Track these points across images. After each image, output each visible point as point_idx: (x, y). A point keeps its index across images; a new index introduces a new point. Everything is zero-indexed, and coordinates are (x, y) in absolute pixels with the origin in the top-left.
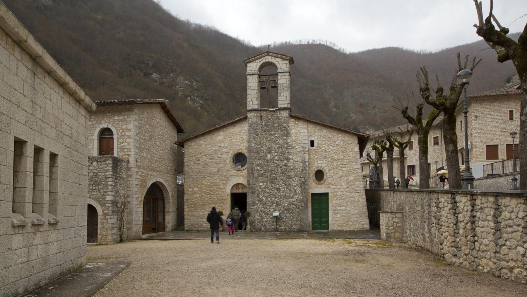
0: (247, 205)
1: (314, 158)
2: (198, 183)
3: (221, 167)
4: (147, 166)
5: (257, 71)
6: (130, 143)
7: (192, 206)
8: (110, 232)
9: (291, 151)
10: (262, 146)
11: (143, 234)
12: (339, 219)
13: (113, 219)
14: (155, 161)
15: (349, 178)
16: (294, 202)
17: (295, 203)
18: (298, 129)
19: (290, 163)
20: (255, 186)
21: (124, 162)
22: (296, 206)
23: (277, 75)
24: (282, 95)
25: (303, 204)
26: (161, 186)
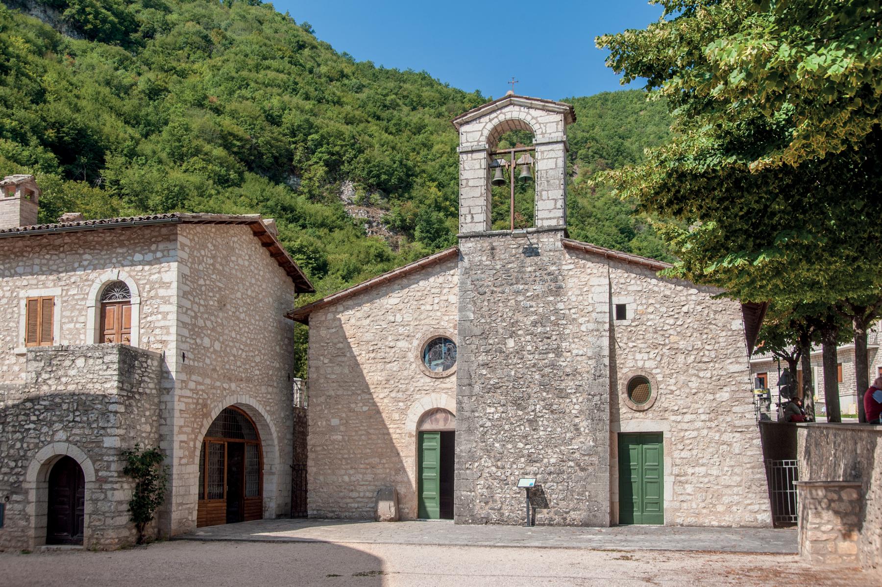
0: (456, 460)
3: (394, 369)
4: (211, 367)
5: (484, 144)
6: (167, 313)
8: (111, 521)
9: (567, 331)
10: (493, 318)
11: (199, 525)
12: (689, 498)
13: (121, 492)
14: (234, 356)
15: (718, 396)
18: (584, 278)
19: (562, 359)
20: (476, 414)
21: (152, 360)
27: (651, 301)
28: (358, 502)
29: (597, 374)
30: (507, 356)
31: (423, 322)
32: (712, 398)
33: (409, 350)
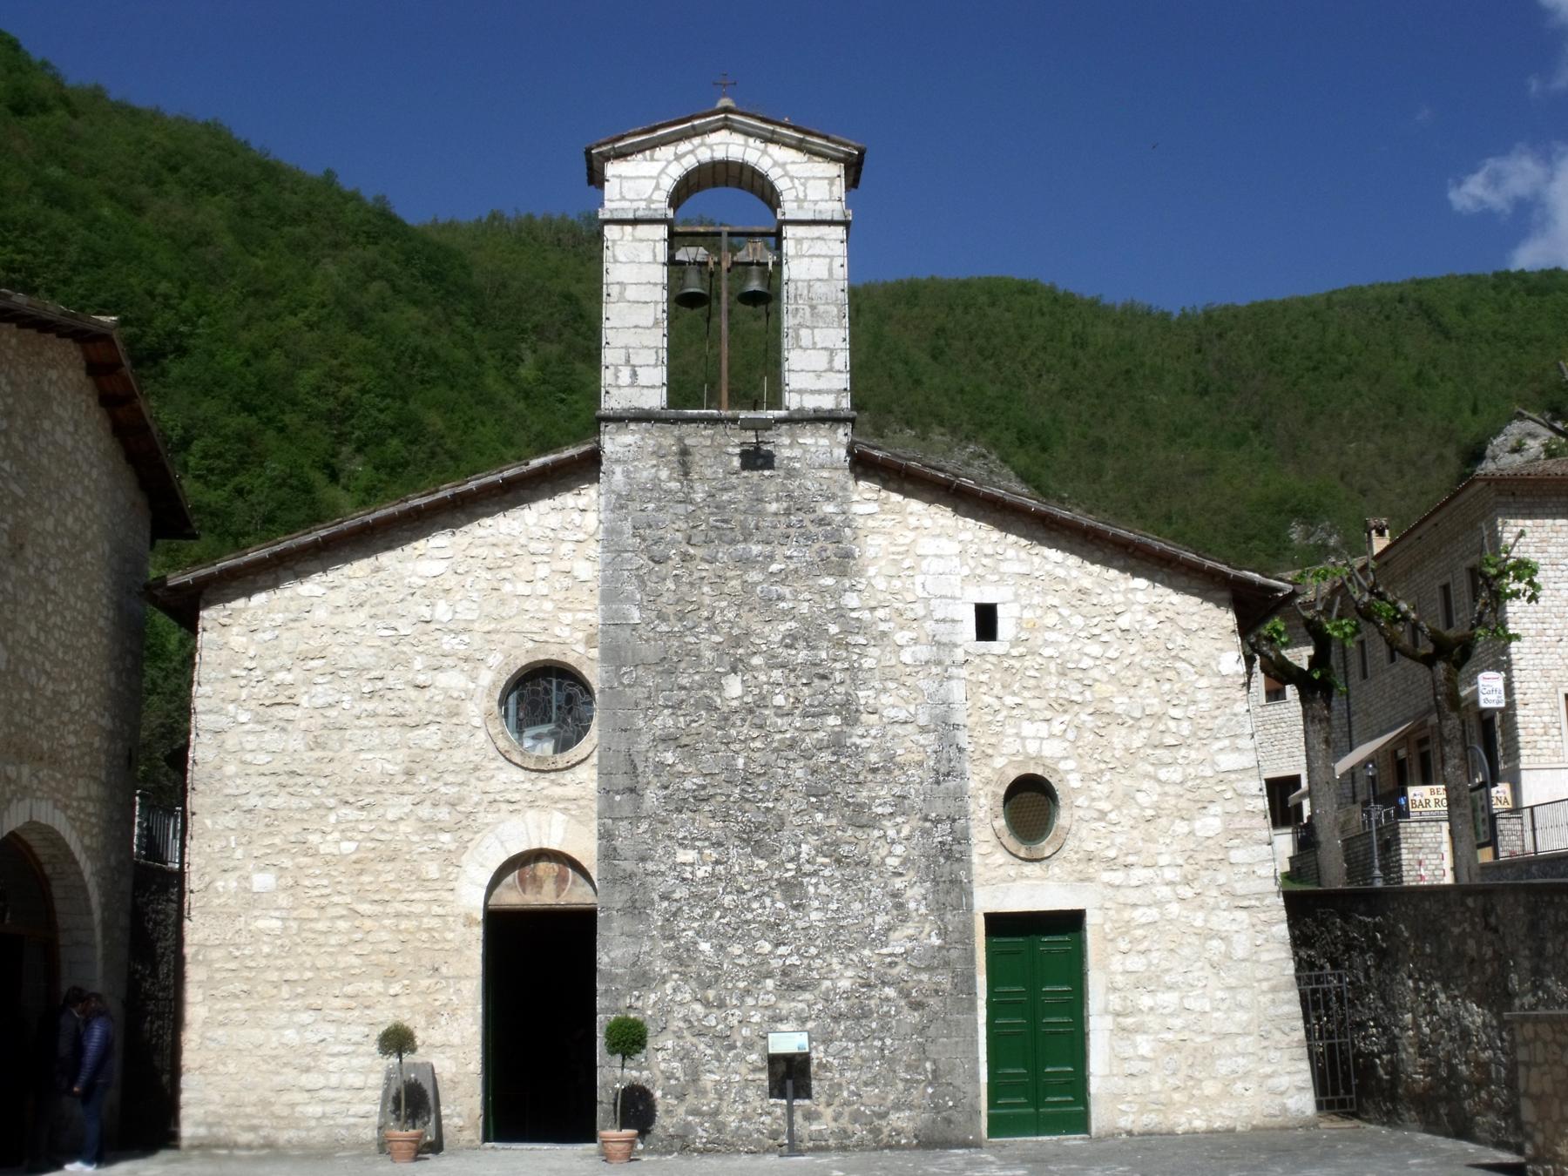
0: (600, 987)
1: (996, 704)
2: (277, 840)
3: (428, 744)
5: (661, 206)
7: (237, 987)
9: (868, 663)
12: (1146, 1066)
15: (1197, 824)
16: (892, 965)
17: (895, 971)
19: (861, 731)
20: (650, 866)
22: (906, 994)
23: (778, 236)
24: (803, 343)
25: (944, 980)
26: (43, 859)
28: (325, 1101)
29: (943, 770)
30: (726, 719)
31: (505, 625)
32: (1186, 830)
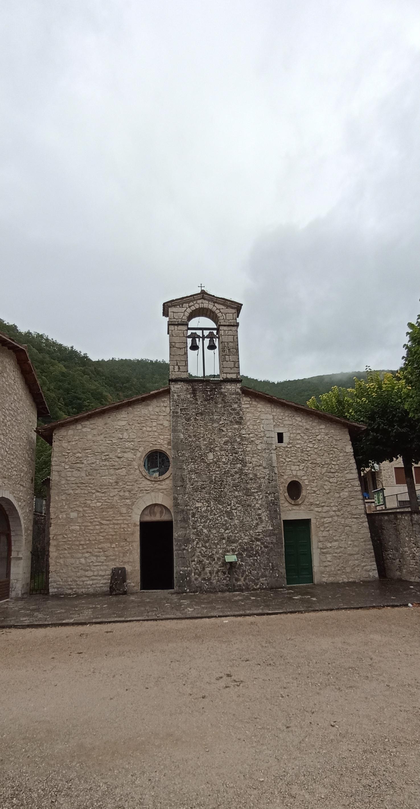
12: (330, 563)
15: (341, 494)
20: (188, 507)
22: (262, 543)
27: (298, 432)
28: (93, 580)
32: (338, 496)
33: (134, 460)
